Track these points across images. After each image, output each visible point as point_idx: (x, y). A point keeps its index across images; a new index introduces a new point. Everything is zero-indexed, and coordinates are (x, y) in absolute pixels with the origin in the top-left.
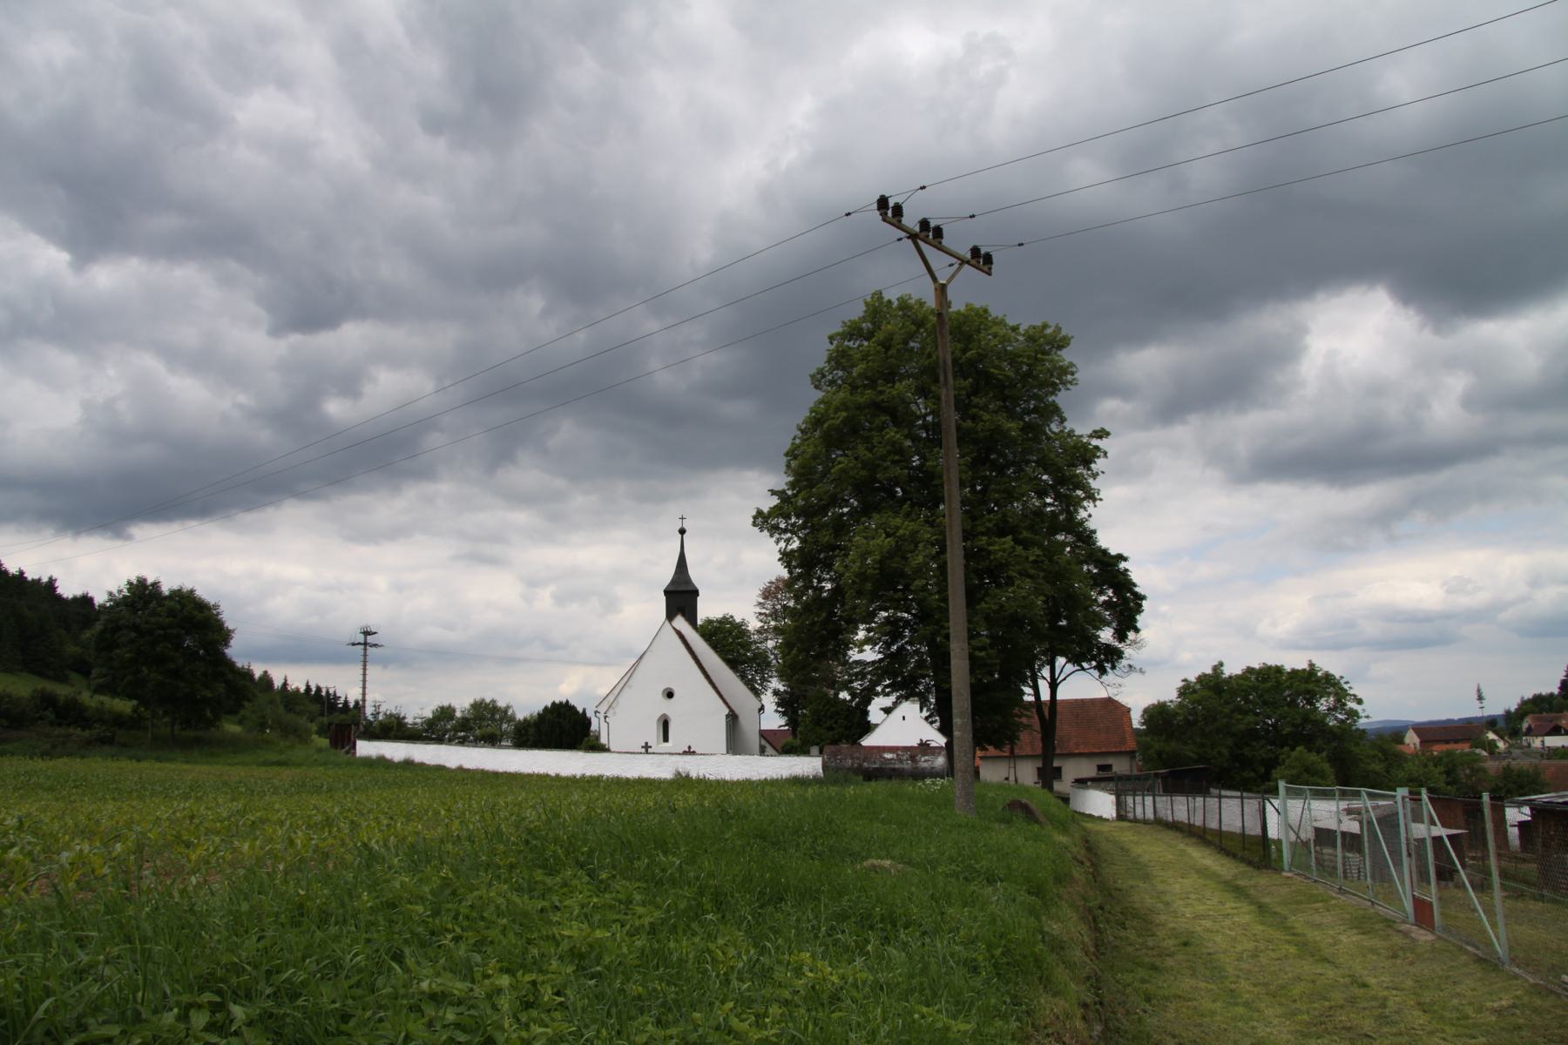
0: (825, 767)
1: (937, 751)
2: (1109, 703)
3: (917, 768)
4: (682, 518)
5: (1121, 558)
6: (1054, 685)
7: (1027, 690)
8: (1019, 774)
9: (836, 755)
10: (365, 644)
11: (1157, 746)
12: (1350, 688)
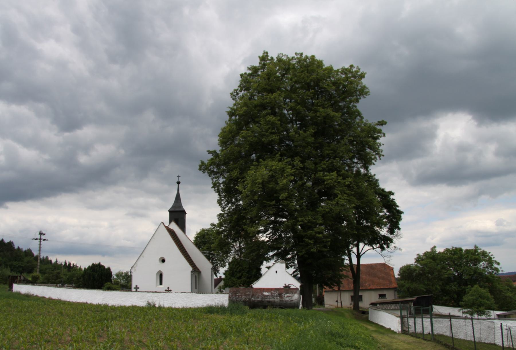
0: (231, 300)
1: (294, 291)
2: (384, 266)
3: (282, 300)
4: (179, 177)
5: (391, 193)
6: (359, 256)
7: (347, 258)
8: (342, 299)
9: (236, 293)
10: (40, 239)
11: (407, 285)
12: (494, 258)
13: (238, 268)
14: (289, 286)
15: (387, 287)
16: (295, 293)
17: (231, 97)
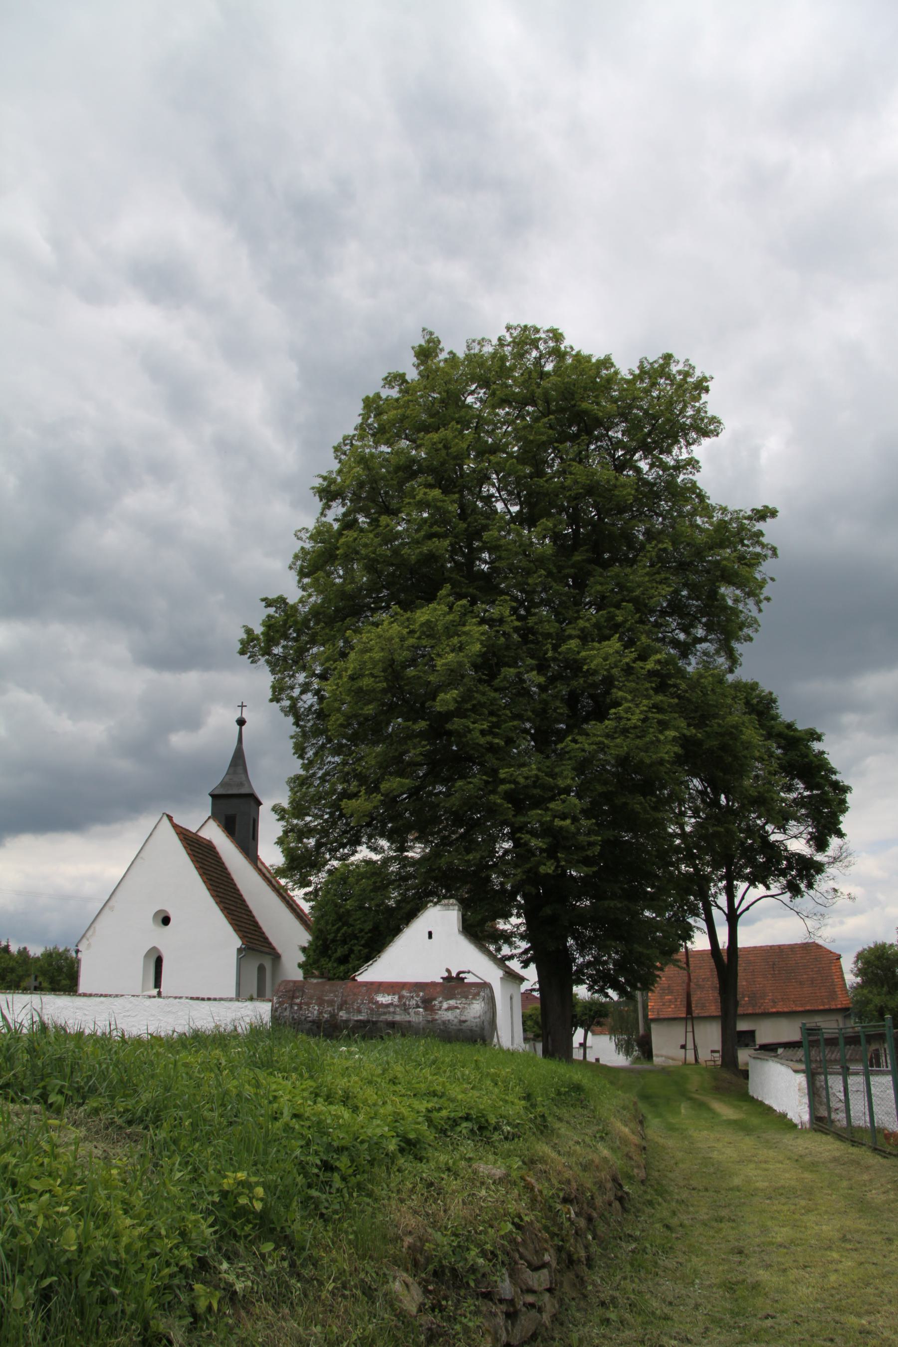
3: (434, 1020)
6: (733, 918)
9: (293, 997)
13: (339, 929)
14: (462, 975)
15: (821, 1007)
16: (474, 998)
17: (336, 458)
